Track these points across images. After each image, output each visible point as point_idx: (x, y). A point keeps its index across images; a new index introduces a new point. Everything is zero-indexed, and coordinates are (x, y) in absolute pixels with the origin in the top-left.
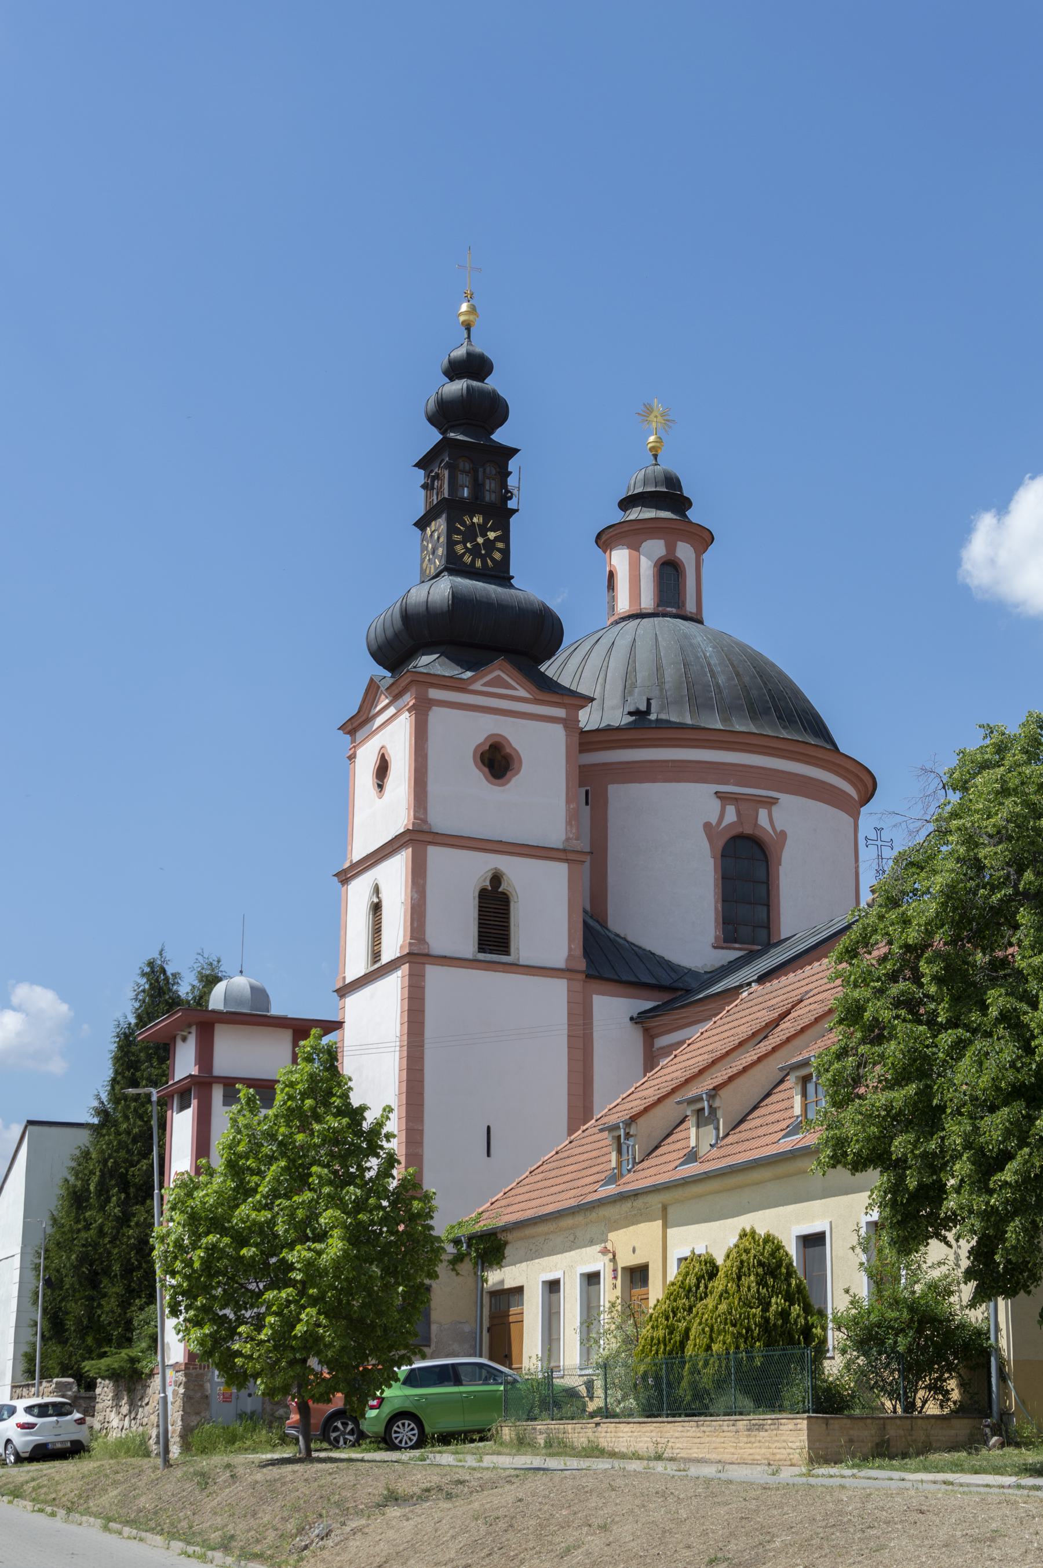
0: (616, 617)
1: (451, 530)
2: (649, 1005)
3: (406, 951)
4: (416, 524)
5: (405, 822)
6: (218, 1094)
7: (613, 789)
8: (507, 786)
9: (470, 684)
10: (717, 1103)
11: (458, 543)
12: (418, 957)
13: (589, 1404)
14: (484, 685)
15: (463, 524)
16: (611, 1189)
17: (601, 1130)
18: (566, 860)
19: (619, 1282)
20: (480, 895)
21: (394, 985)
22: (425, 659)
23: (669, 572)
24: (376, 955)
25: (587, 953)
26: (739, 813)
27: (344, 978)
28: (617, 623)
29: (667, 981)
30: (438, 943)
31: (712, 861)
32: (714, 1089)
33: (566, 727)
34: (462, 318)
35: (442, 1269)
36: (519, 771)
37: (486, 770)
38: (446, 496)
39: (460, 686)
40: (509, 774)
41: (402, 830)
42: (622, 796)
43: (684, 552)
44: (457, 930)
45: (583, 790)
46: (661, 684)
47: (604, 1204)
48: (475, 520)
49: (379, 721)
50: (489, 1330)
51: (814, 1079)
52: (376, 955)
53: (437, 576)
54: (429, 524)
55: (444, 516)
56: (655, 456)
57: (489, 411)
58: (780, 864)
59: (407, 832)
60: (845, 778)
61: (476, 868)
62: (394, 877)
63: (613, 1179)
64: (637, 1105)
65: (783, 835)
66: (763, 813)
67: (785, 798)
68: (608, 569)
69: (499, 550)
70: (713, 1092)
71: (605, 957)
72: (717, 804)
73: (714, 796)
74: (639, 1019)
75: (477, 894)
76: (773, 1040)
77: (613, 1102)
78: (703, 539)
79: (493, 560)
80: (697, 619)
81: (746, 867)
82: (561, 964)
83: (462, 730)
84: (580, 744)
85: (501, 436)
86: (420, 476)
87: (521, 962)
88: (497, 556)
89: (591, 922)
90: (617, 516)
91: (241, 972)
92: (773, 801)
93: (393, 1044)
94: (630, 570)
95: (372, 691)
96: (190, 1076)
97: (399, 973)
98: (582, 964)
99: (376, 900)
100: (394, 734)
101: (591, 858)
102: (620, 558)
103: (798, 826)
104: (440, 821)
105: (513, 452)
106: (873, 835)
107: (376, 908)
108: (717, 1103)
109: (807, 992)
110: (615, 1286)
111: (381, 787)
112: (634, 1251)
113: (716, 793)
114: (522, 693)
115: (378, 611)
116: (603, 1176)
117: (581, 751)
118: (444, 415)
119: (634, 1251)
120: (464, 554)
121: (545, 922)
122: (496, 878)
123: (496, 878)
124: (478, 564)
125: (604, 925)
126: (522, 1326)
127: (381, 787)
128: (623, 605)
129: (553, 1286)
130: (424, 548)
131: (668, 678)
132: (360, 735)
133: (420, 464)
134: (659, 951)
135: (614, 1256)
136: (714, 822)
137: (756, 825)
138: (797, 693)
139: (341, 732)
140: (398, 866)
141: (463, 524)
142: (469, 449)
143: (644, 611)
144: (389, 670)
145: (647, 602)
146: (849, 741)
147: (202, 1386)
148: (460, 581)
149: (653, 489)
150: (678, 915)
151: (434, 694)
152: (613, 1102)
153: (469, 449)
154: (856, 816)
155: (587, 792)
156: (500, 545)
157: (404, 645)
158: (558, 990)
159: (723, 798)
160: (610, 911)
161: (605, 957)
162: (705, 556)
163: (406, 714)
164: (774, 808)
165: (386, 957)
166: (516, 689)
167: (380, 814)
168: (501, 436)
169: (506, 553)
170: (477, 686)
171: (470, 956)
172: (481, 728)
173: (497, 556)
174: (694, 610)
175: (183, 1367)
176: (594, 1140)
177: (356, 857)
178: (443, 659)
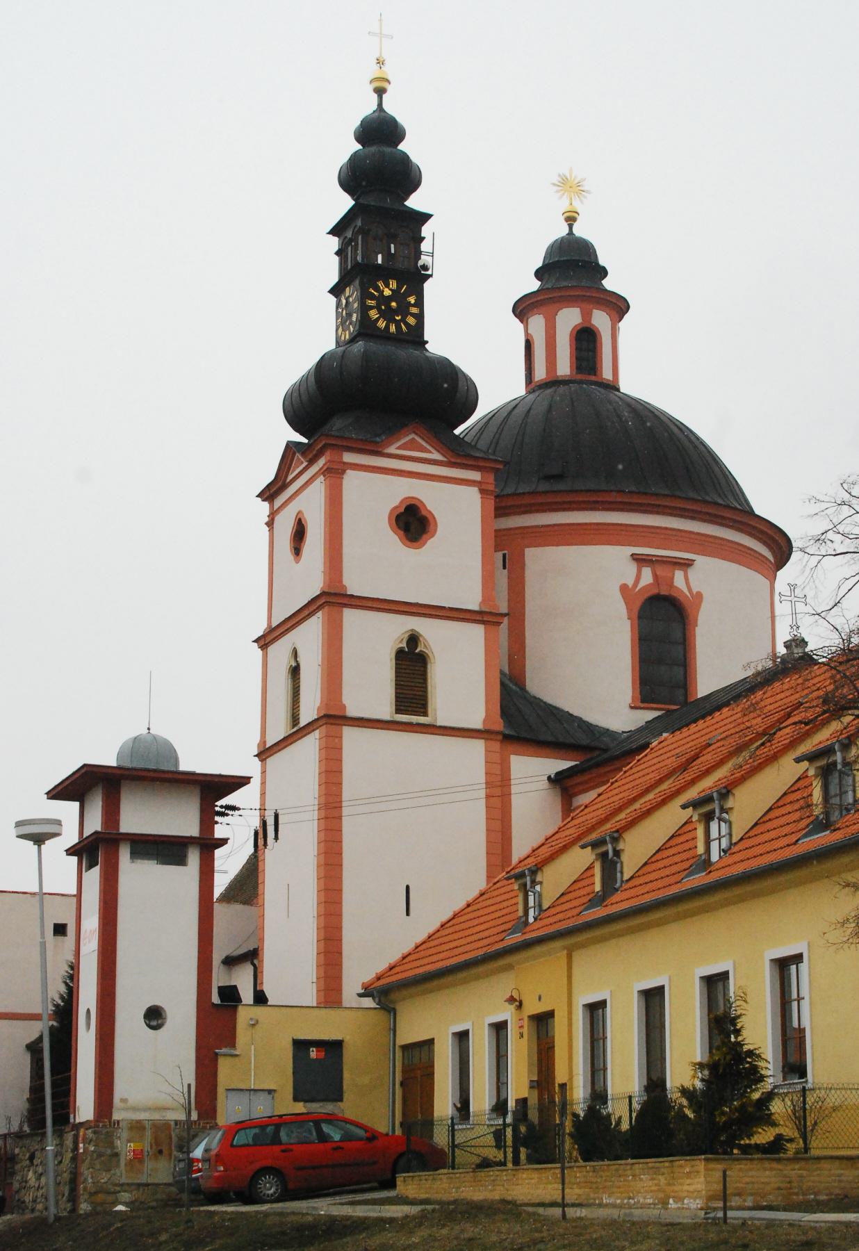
1: (365, 295)
2: (565, 765)
4: (331, 291)
6: (124, 854)
7: (530, 553)
10: (621, 846)
11: (372, 308)
13: (349, 1107)
14: (398, 448)
18: (483, 622)
19: (525, 1030)
21: (310, 746)
24: (295, 719)
25: (505, 713)
26: (655, 576)
29: (585, 741)
31: (629, 622)
33: (482, 491)
36: (435, 531)
40: (425, 536)
42: (538, 559)
43: (600, 320)
44: (371, 691)
45: (499, 555)
50: (402, 1084)
51: (717, 814)
52: (295, 719)
54: (343, 291)
55: (357, 282)
59: (323, 594)
60: (759, 540)
61: (394, 629)
65: (699, 596)
67: (701, 561)
69: (413, 315)
71: (523, 720)
72: (632, 568)
74: (559, 781)
78: (618, 307)
79: (407, 325)
81: (663, 627)
82: (477, 722)
84: (496, 509)
85: (415, 202)
86: (335, 243)
87: (439, 724)
89: (507, 682)
92: (686, 565)
96: (96, 832)
98: (499, 725)
101: (504, 618)
103: (714, 584)
104: (355, 584)
105: (425, 217)
107: (295, 671)
108: (621, 846)
110: (522, 1036)
111: (297, 551)
114: (436, 456)
116: (509, 925)
120: (377, 320)
122: (413, 639)
123: (413, 639)
124: (393, 328)
125: (523, 688)
127: (297, 551)
129: (462, 1037)
133: (335, 231)
134: (576, 712)
136: (630, 583)
140: (314, 628)
146: (764, 502)
147: (112, 1143)
148: (374, 346)
150: (597, 683)
154: (772, 579)
155: (504, 556)
156: (414, 310)
159: (640, 560)
160: (528, 675)
161: (523, 720)
162: (621, 324)
163: (322, 478)
164: (691, 571)
165: (303, 721)
168: (415, 202)
169: (420, 317)
170: (392, 450)
171: (387, 717)
172: (397, 491)
174: (610, 378)
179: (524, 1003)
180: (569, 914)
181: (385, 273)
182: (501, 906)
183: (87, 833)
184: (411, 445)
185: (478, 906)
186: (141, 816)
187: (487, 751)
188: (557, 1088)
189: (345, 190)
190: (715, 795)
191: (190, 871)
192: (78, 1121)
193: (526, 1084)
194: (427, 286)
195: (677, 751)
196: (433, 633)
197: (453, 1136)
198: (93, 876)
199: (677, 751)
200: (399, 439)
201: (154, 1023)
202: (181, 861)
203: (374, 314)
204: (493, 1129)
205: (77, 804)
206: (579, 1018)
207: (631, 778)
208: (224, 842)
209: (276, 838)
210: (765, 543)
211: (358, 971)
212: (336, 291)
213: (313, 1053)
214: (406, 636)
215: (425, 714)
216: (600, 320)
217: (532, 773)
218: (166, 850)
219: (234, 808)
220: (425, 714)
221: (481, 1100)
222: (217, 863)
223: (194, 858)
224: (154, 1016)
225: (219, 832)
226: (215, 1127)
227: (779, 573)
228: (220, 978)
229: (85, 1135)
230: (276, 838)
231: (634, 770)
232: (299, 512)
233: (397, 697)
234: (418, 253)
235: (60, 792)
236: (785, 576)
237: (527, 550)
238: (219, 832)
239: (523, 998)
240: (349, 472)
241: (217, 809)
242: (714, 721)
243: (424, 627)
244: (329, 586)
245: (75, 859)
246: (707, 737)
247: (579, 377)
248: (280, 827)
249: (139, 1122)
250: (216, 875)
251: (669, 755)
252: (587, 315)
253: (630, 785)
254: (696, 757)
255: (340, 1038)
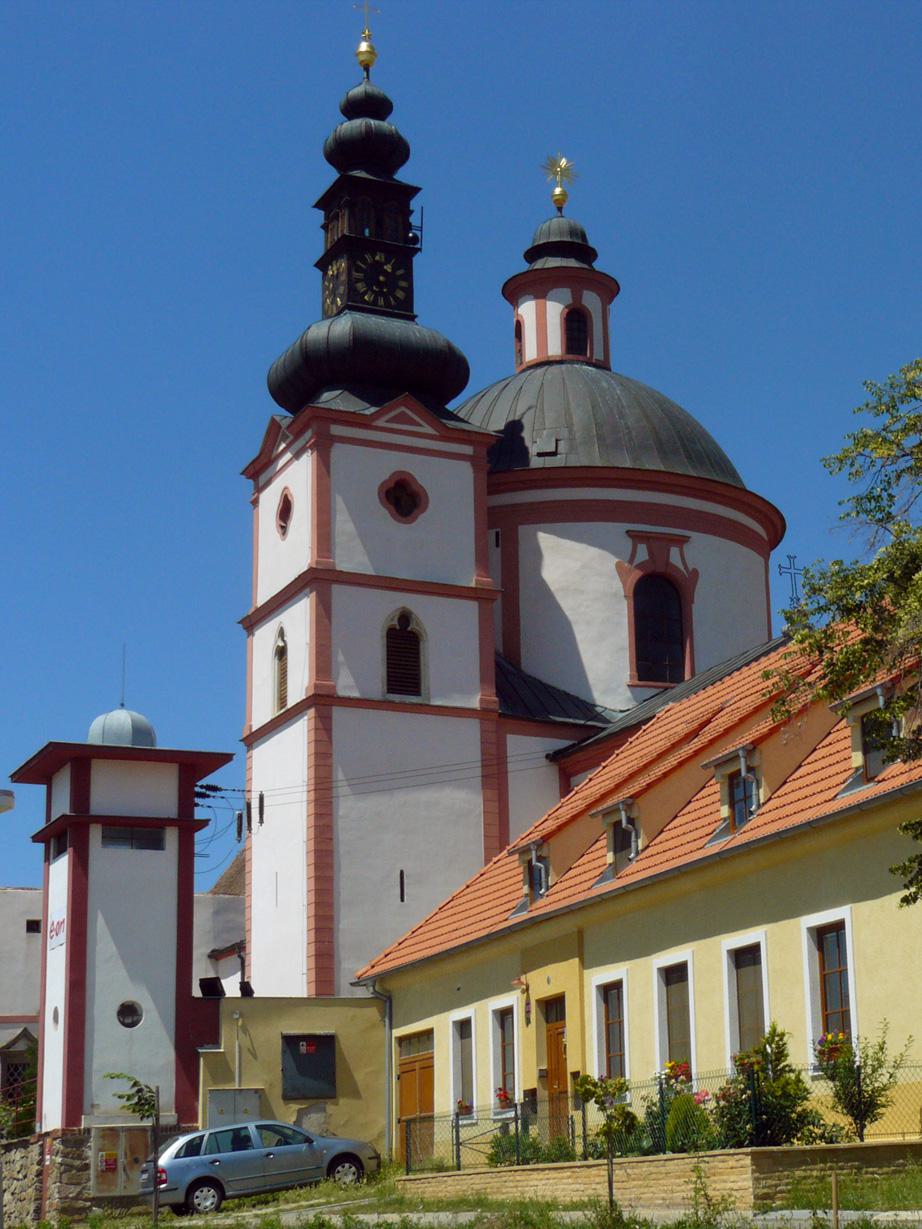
0: (524, 366)
2: (562, 744)
3: (311, 692)
5: (309, 561)
6: (95, 833)
8: (413, 525)
9: (374, 420)
12: (322, 701)
14: (387, 421)
15: (364, 261)
16: (524, 916)
17: (511, 854)
20: (387, 633)
22: (326, 396)
23: (577, 327)
24: (282, 699)
26: (651, 553)
27: (251, 727)
28: (524, 371)
30: (346, 685)
32: (631, 797)
34: (362, 58)
35: (899, 1218)
37: (392, 507)
38: (346, 232)
39: (364, 422)
40: (416, 511)
41: (306, 569)
43: (591, 300)
44: (362, 672)
45: (492, 533)
46: (570, 427)
47: (516, 932)
48: (377, 258)
49: (281, 462)
52: (282, 699)
53: (339, 313)
56: (560, 209)
57: (391, 151)
58: (693, 602)
59: (311, 570)
61: (385, 607)
62: (298, 619)
63: (522, 908)
64: (551, 825)
65: (695, 573)
66: (674, 552)
67: (696, 537)
68: (515, 320)
69: (403, 289)
70: (630, 801)
73: (625, 535)
75: (385, 633)
76: (696, 744)
77: (526, 827)
78: (608, 288)
80: (603, 365)
83: (368, 467)
85: (404, 175)
86: (320, 215)
88: (400, 294)
90: (524, 267)
91: (122, 705)
92: (681, 541)
93: (300, 789)
94: (541, 323)
95: (274, 432)
96: (63, 816)
97: (306, 718)
99: (281, 644)
100: (297, 475)
102: (527, 310)
105: (415, 190)
106: (785, 563)
107: (281, 653)
109: (727, 701)
111: (284, 529)
112: (549, 981)
113: (627, 532)
115: (276, 350)
117: (490, 493)
118: (341, 153)
119: (549, 981)
121: (455, 668)
122: (405, 617)
123: (405, 617)
124: (381, 301)
126: (433, 1070)
127: (284, 529)
128: (531, 354)
130: (325, 288)
131: (575, 420)
132: (262, 479)
135: (527, 990)
137: (668, 563)
138: (704, 435)
139: (243, 477)
141: (364, 261)
142: (369, 203)
143: (551, 359)
144: (291, 413)
145: (555, 347)
146: (754, 480)
148: (358, 316)
149: (558, 239)
151: (337, 430)
152: (526, 827)
153: (369, 203)
154: (767, 559)
156: (403, 284)
157: (303, 384)
158: (472, 730)
159: (636, 537)
162: (612, 307)
164: (686, 547)
166: (420, 425)
167: (282, 556)
168: (404, 175)
169: (409, 291)
170: (381, 423)
172: (389, 464)
173: (400, 294)
174: (601, 358)
175: (60, 1134)
176: (510, 868)
177: (261, 599)
178: (346, 393)
179: (530, 988)
180: (580, 888)
181: (372, 246)
182: (504, 884)
183: (53, 819)
184: (401, 418)
185: (476, 888)
186: (112, 792)
187: (483, 731)
188: (569, 1076)
189: (331, 164)
190: (741, 753)
191: (166, 859)
192: (44, 1131)
193: (535, 1074)
194: (417, 260)
195: (688, 717)
196: (430, 614)
197: (457, 1132)
198: (61, 869)
199: (688, 717)
200: (391, 409)
201: (128, 1020)
202: (157, 844)
203: (361, 287)
204: (500, 1124)
205: (43, 788)
206: (592, 999)
207: (638, 748)
208: (204, 823)
209: (261, 821)
210: (762, 523)
211: (352, 966)
212: (323, 264)
213: (303, 1048)
214: (398, 614)
215: (417, 692)
216: (591, 300)
217: (527, 751)
218: (140, 832)
219: (214, 789)
220: (417, 692)
221: (485, 1095)
222: (197, 849)
223: (171, 837)
224: (129, 1014)
225: (199, 814)
226: (524, 851)
227: (772, 553)
228: (201, 970)
229: (52, 1145)
230: (261, 821)
231: (641, 740)
232: (286, 488)
233: (388, 676)
234: (409, 227)
235: (24, 775)
236: (778, 556)
237: (520, 527)
238: (199, 814)
239: (530, 982)
240: (337, 445)
241: (197, 789)
242: (733, 681)
243: (415, 603)
244: (317, 563)
245: (41, 846)
246: (718, 702)
247: (570, 356)
248: (265, 809)
249: (112, 1129)
250: (197, 860)
251: (659, 738)
252: (577, 297)
253: (666, 734)
254: (708, 722)
255: (331, 1031)
